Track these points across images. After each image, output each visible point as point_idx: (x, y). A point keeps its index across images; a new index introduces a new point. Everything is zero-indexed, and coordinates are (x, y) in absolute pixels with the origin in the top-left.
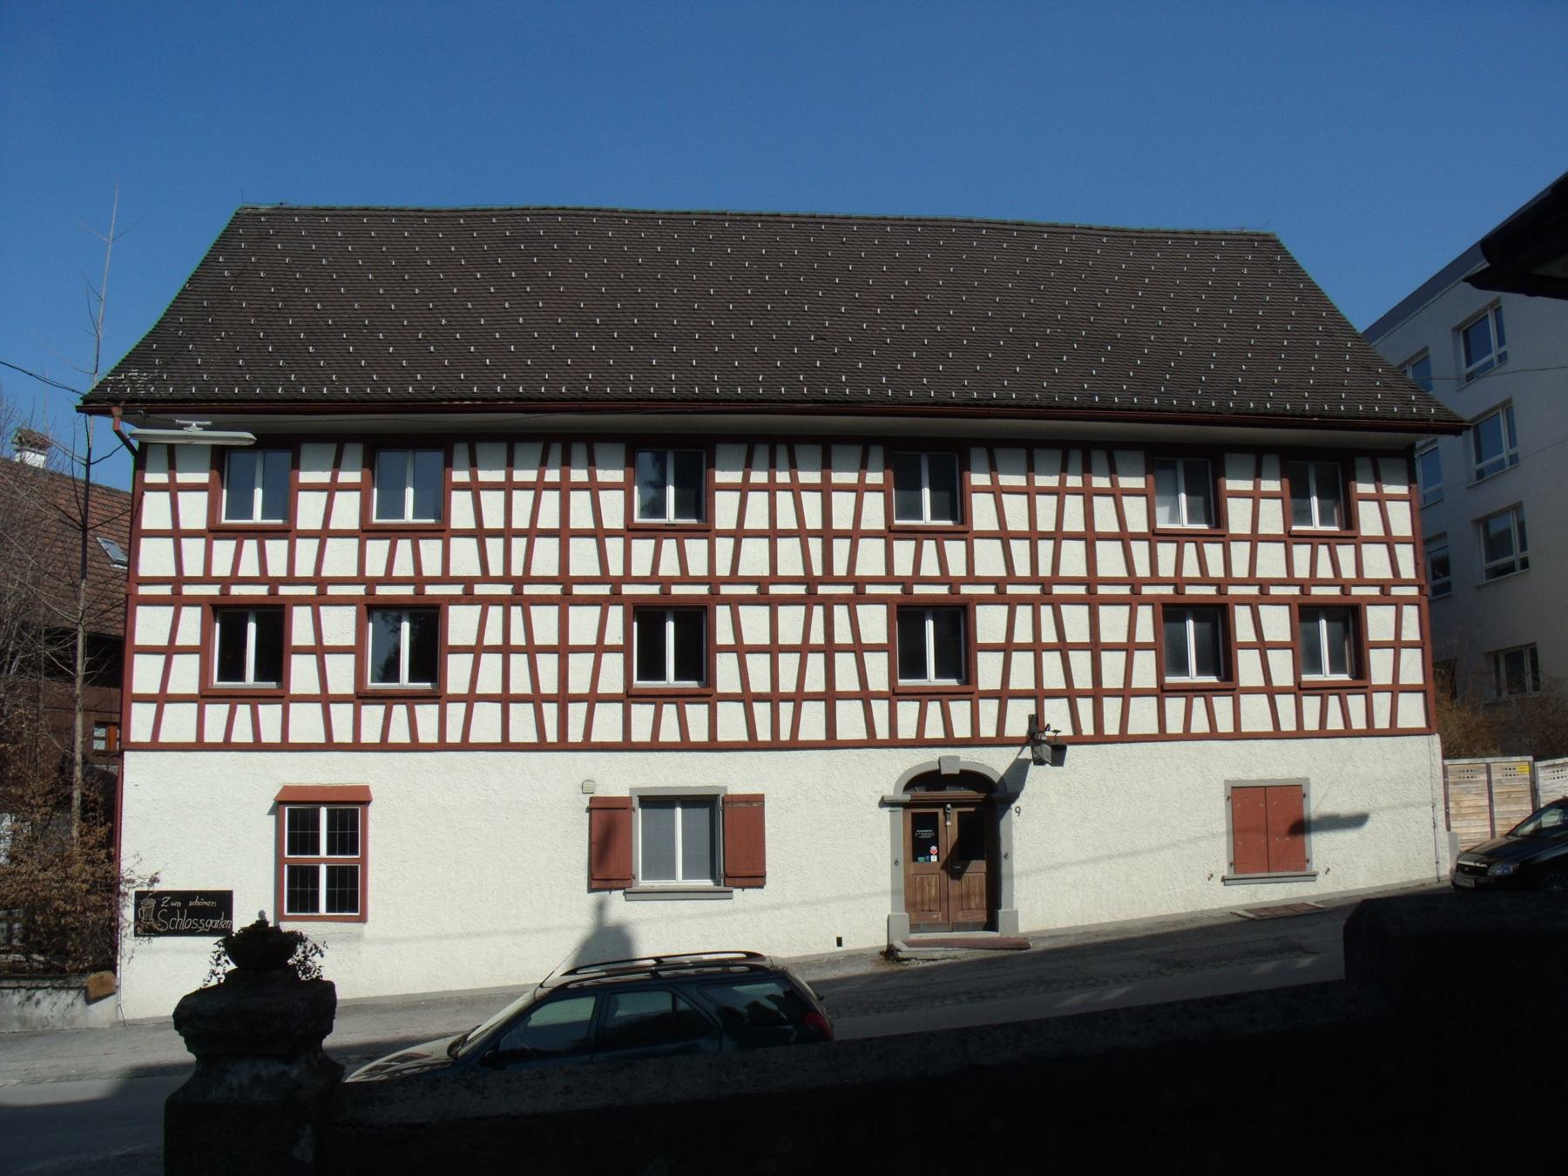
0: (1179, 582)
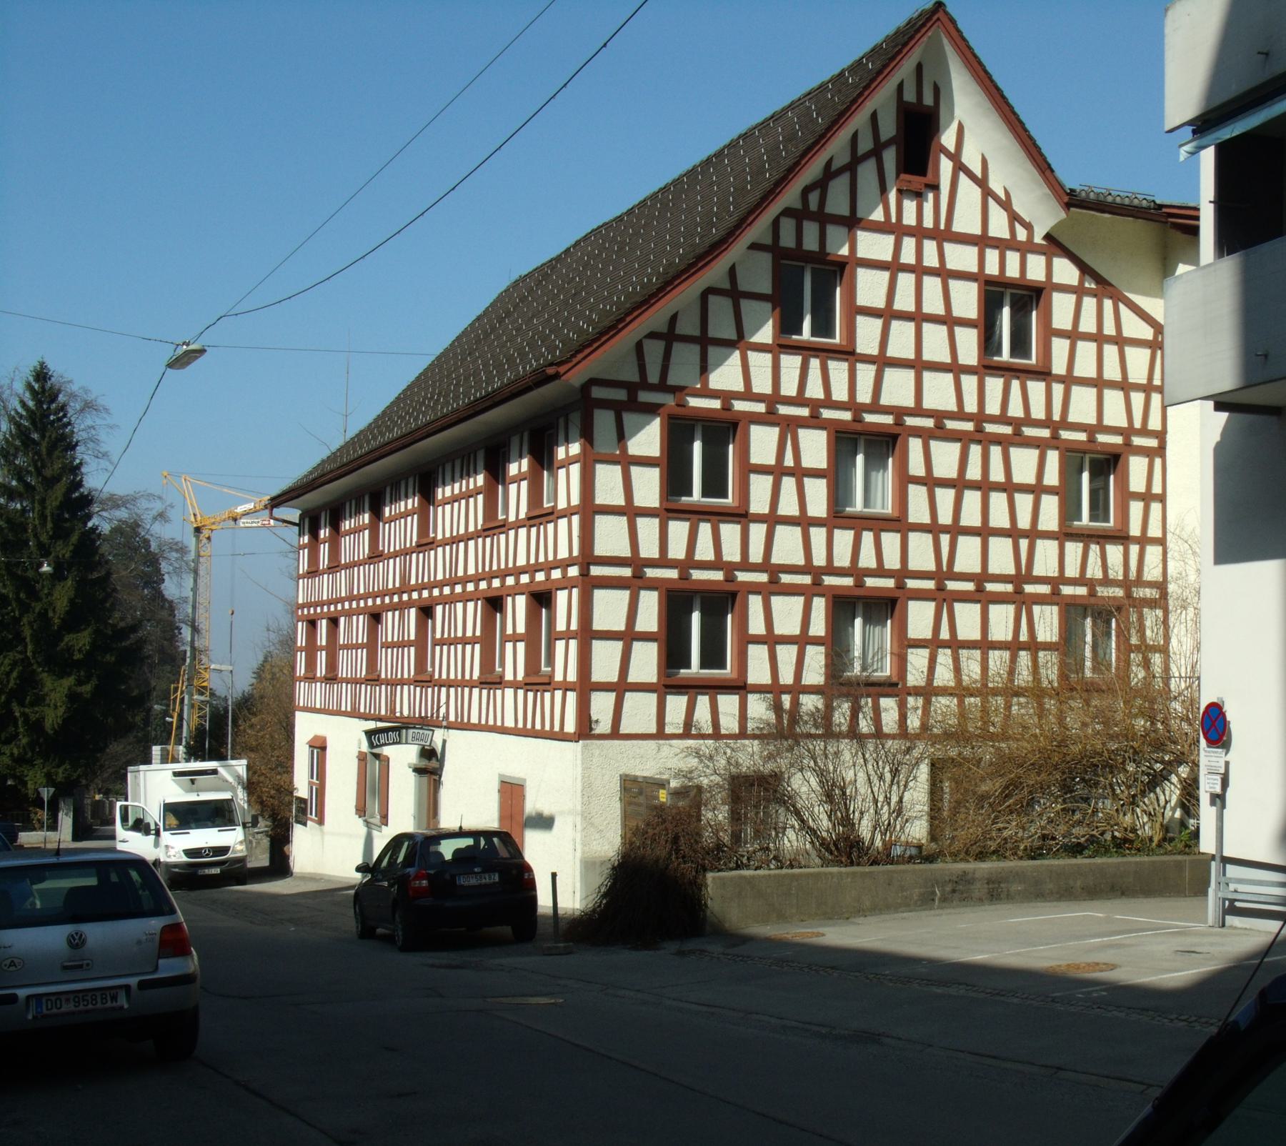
0: (689, 563)
